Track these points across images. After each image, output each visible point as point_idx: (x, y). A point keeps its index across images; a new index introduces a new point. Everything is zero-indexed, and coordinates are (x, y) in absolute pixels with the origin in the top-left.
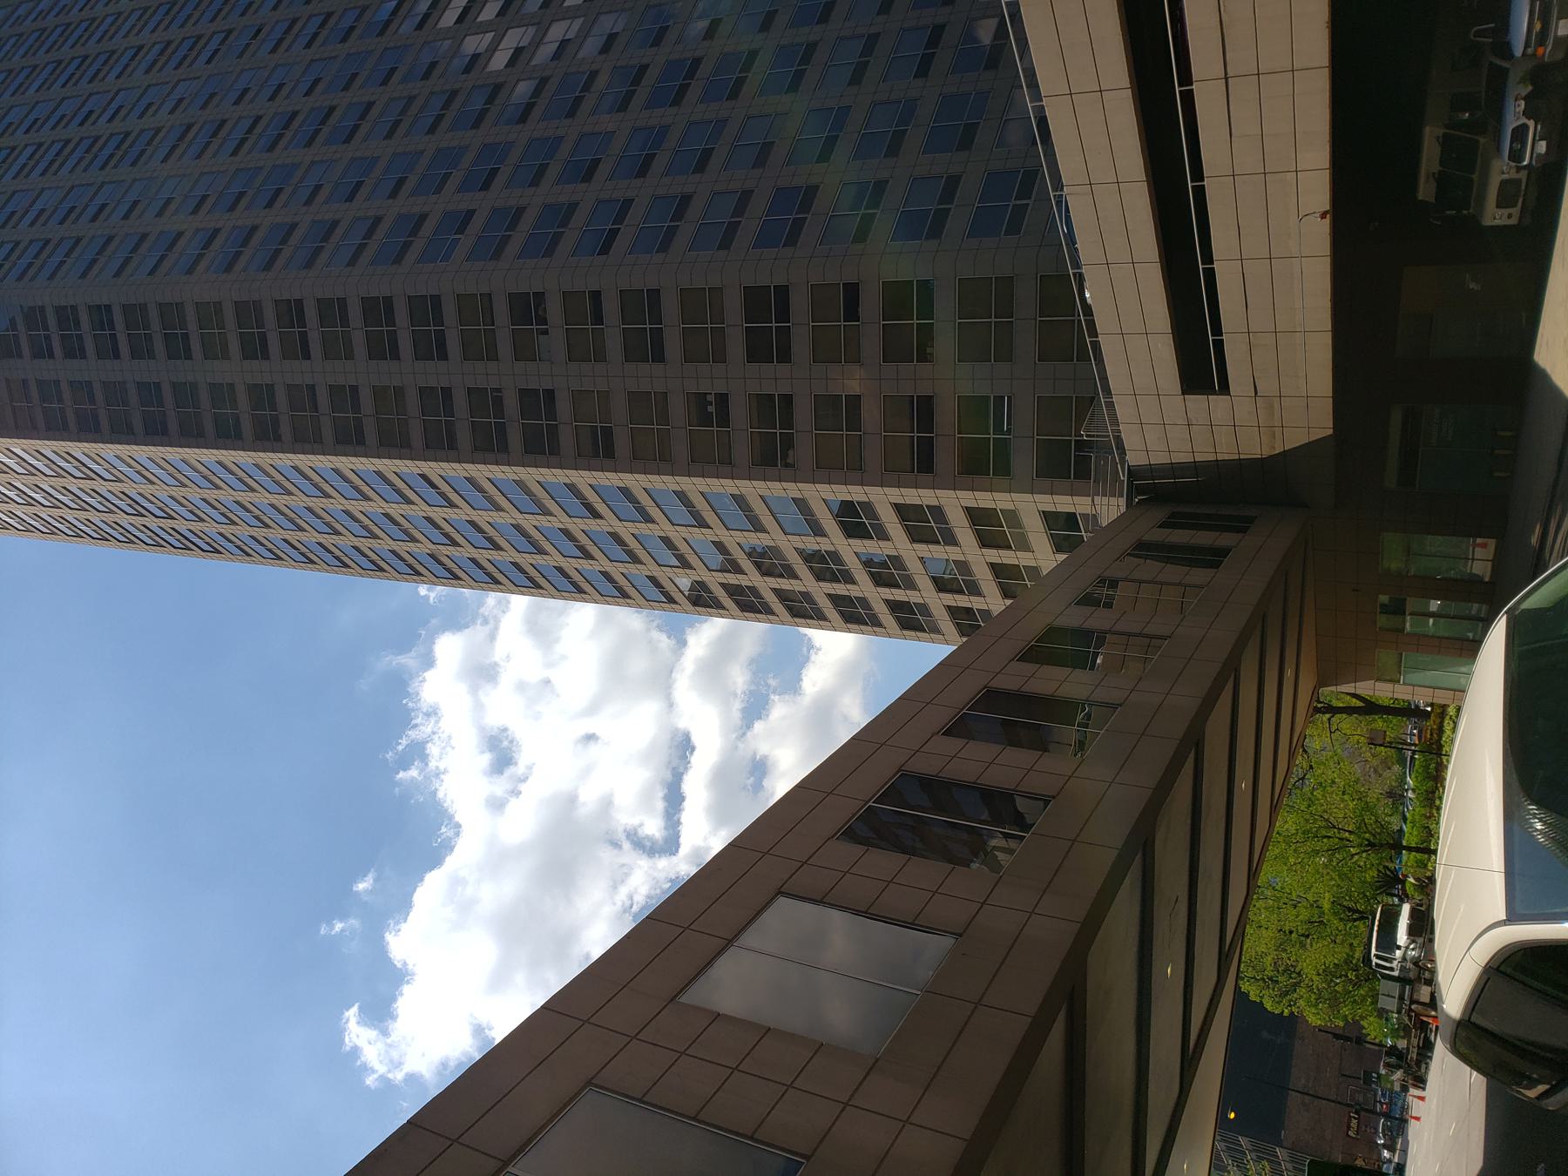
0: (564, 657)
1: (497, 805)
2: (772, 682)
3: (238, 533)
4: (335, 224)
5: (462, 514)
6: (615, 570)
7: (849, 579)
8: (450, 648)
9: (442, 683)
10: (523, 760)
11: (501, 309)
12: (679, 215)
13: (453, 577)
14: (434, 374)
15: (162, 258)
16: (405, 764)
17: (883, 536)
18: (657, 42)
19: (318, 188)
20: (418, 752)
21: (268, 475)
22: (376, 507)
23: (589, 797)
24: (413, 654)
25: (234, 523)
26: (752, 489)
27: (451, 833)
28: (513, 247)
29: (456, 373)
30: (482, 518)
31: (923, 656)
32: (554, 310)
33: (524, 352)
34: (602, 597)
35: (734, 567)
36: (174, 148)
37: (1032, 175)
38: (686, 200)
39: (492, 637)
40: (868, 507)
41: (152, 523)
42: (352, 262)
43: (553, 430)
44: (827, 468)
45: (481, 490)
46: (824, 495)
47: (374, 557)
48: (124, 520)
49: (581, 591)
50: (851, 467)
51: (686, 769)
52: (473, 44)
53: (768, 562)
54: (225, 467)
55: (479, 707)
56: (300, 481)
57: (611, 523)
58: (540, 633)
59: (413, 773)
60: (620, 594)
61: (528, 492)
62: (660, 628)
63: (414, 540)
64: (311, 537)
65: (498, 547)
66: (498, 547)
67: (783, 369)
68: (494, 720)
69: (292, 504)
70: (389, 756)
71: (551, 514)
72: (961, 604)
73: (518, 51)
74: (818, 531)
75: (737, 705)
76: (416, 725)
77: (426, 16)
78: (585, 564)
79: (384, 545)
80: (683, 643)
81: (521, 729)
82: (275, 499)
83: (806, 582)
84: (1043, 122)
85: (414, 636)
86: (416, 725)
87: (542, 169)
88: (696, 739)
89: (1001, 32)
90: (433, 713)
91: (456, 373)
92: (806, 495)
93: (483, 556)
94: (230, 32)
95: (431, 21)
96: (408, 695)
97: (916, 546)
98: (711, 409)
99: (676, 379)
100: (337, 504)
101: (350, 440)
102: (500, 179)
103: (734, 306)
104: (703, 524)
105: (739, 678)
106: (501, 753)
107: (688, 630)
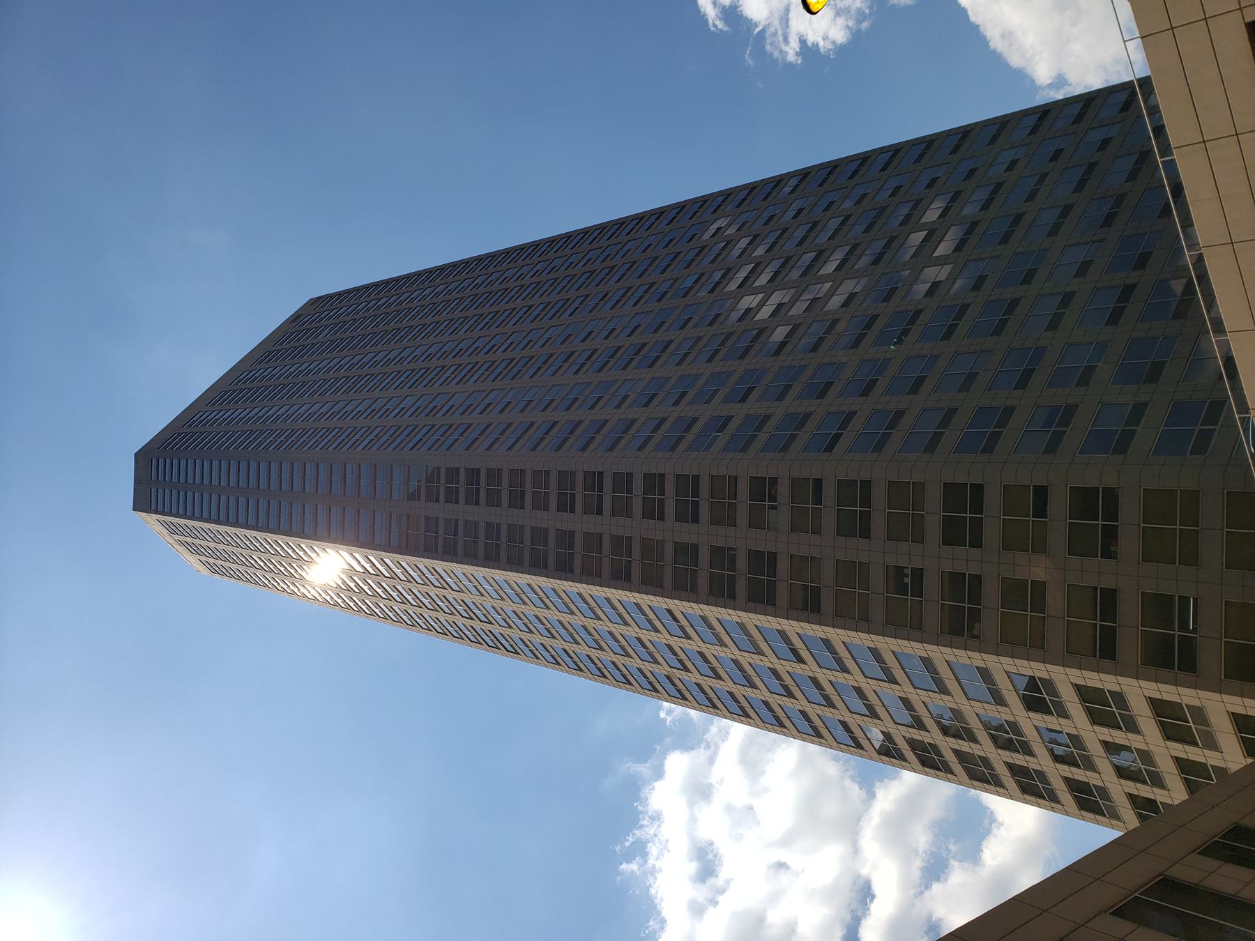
0: (766, 790)
1: (697, 910)
2: (952, 847)
3: (533, 640)
4: (634, 421)
5: (694, 645)
6: (812, 711)
7: (1027, 750)
8: (677, 764)
9: (666, 795)
10: (724, 874)
11: (743, 490)
12: (893, 424)
13: (681, 697)
14: (687, 533)
15: (518, 439)
16: (629, 859)
17: (1063, 713)
18: (887, 299)
19: (626, 397)
20: (639, 850)
21: (560, 597)
22: (632, 632)
23: (775, 917)
24: (648, 764)
25: (531, 632)
26: (941, 654)
27: (656, 927)
28: (756, 445)
29: (703, 535)
30: (709, 650)
31: (1095, 835)
32: (784, 490)
33: (757, 522)
34: (800, 734)
35: (919, 724)
36: (539, 369)
37: (1219, 405)
38: (900, 414)
39: (711, 761)
40: (1049, 685)
41: (477, 625)
42: (641, 448)
43: (772, 585)
44: (1010, 643)
45: (710, 627)
46: (1009, 669)
47: (626, 672)
48: (460, 621)
49: (782, 725)
50: (1036, 647)
51: (865, 915)
52: (749, 301)
53: (956, 729)
54: (532, 589)
55: (693, 820)
56: (614, 671)
57: (811, 669)
58: (751, 764)
59: (634, 867)
60: (814, 733)
61: (747, 633)
62: (853, 778)
63: (656, 662)
64: (582, 650)
65: (718, 677)
66: (718, 677)
67: (974, 553)
68: (704, 834)
69: (573, 622)
70: (618, 848)
71: (764, 655)
72: (1143, 794)
73: (780, 306)
74: (999, 700)
75: (918, 864)
76: (642, 826)
77: (718, 284)
78: (786, 702)
79: (634, 663)
80: (872, 795)
81: (724, 847)
82: (562, 617)
83: (985, 748)
84: (1230, 362)
85: (651, 747)
86: (642, 826)
87: (788, 388)
88: (876, 888)
89: (1189, 286)
90: (656, 817)
91: (703, 535)
92: (990, 665)
93: (707, 682)
94: (587, 296)
95: (721, 286)
96: (639, 799)
97: (1097, 728)
98: (908, 580)
99: (879, 553)
100: (604, 626)
101: (620, 578)
102: (754, 395)
103: (934, 498)
104: (892, 680)
105: (922, 839)
106: (706, 864)
107: (878, 784)
